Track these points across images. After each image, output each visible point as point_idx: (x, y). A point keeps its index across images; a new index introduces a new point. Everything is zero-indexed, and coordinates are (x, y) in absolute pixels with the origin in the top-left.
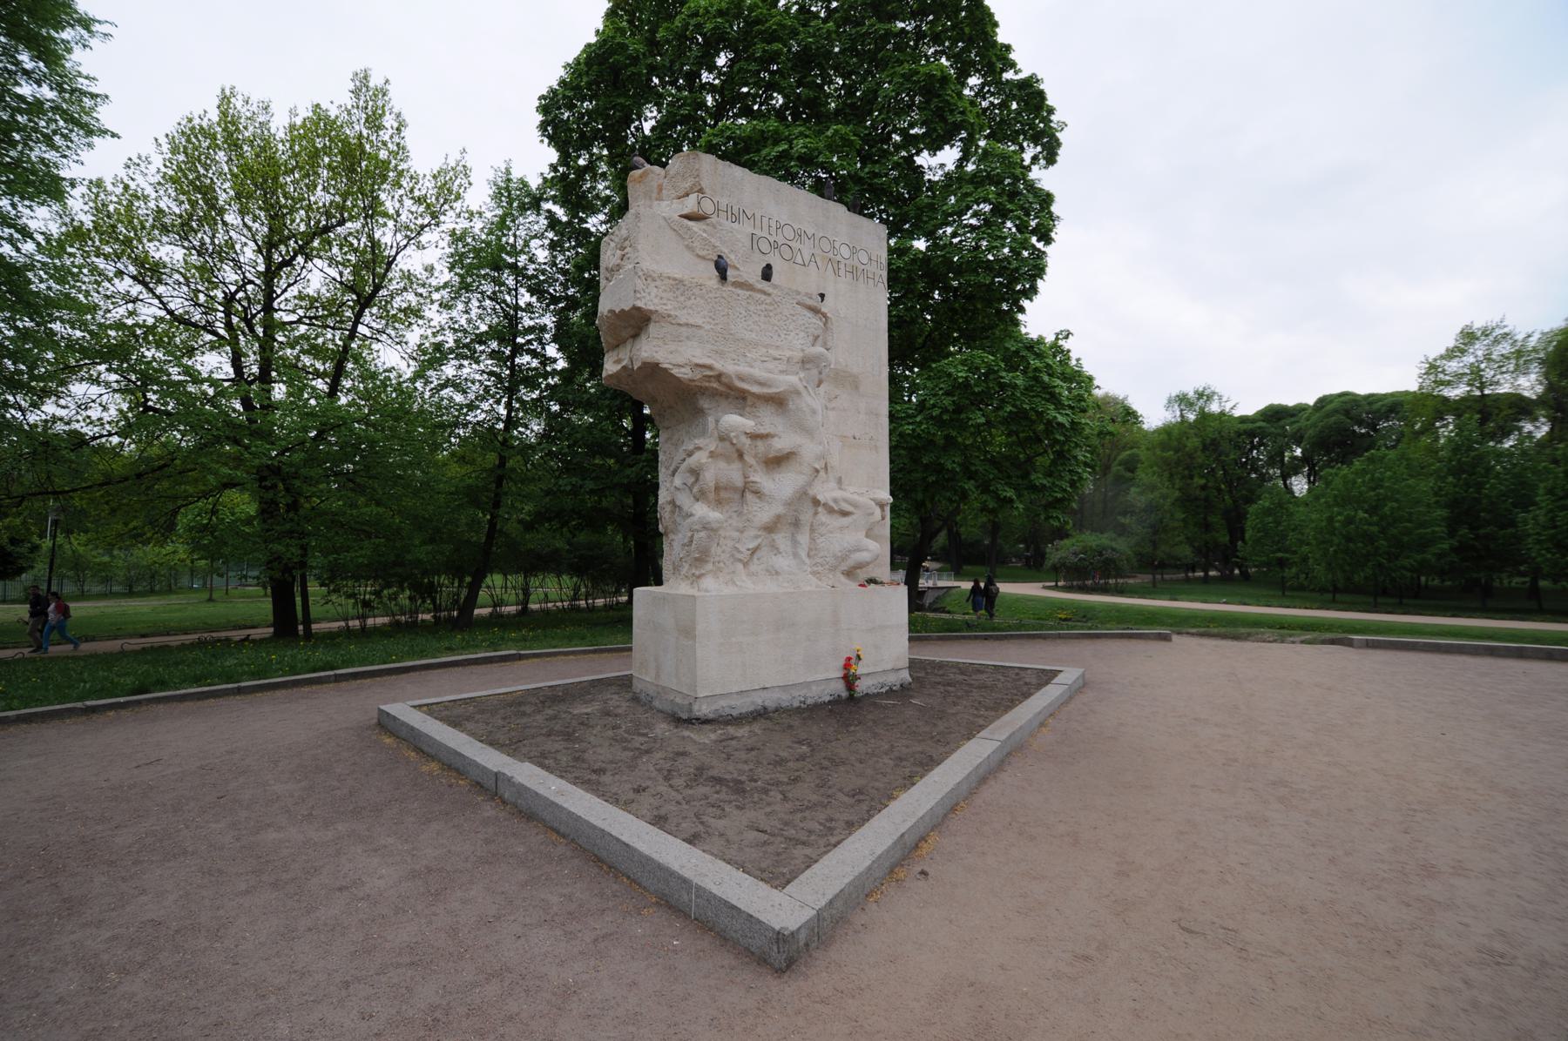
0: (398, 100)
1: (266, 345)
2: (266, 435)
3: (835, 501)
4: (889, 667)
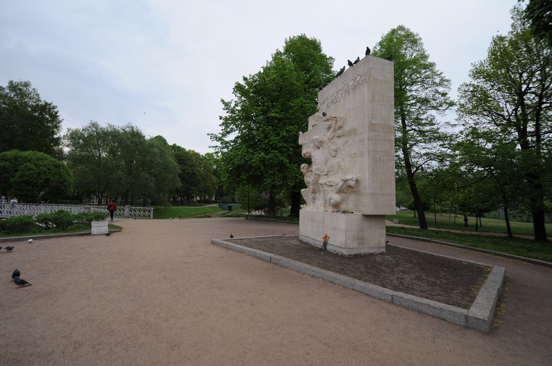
3: (329, 182)
4: (338, 245)
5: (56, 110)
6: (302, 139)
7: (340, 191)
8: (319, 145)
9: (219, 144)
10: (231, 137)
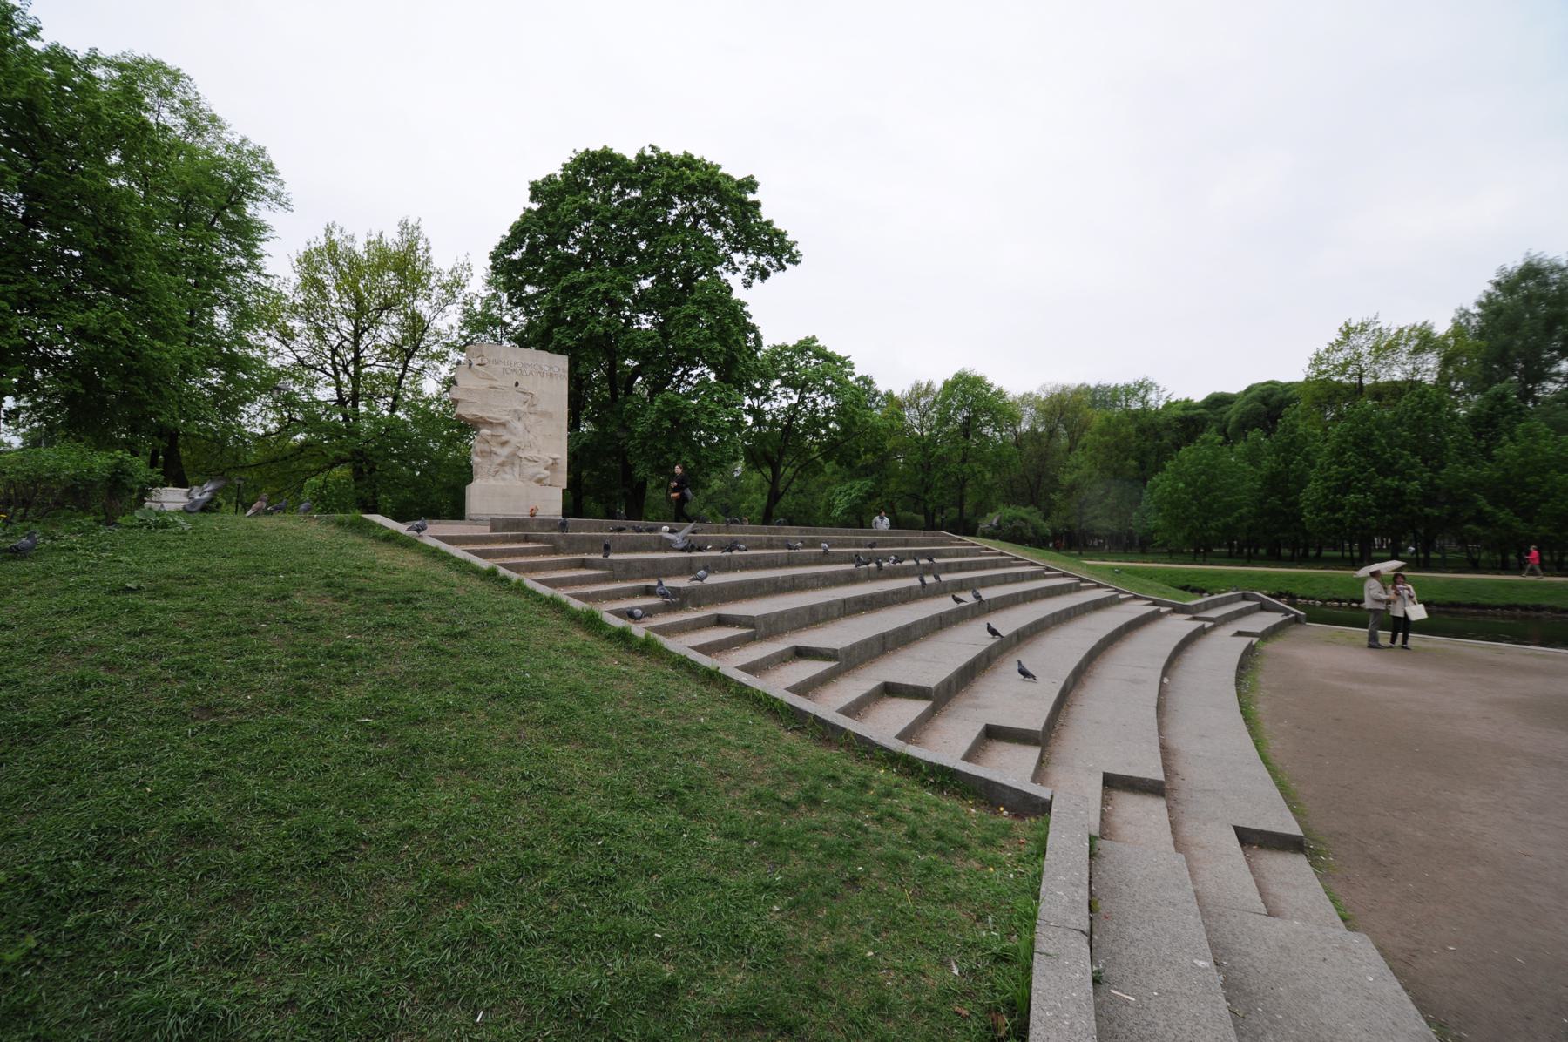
0: (426, 231)
1: (355, 380)
2: (356, 434)
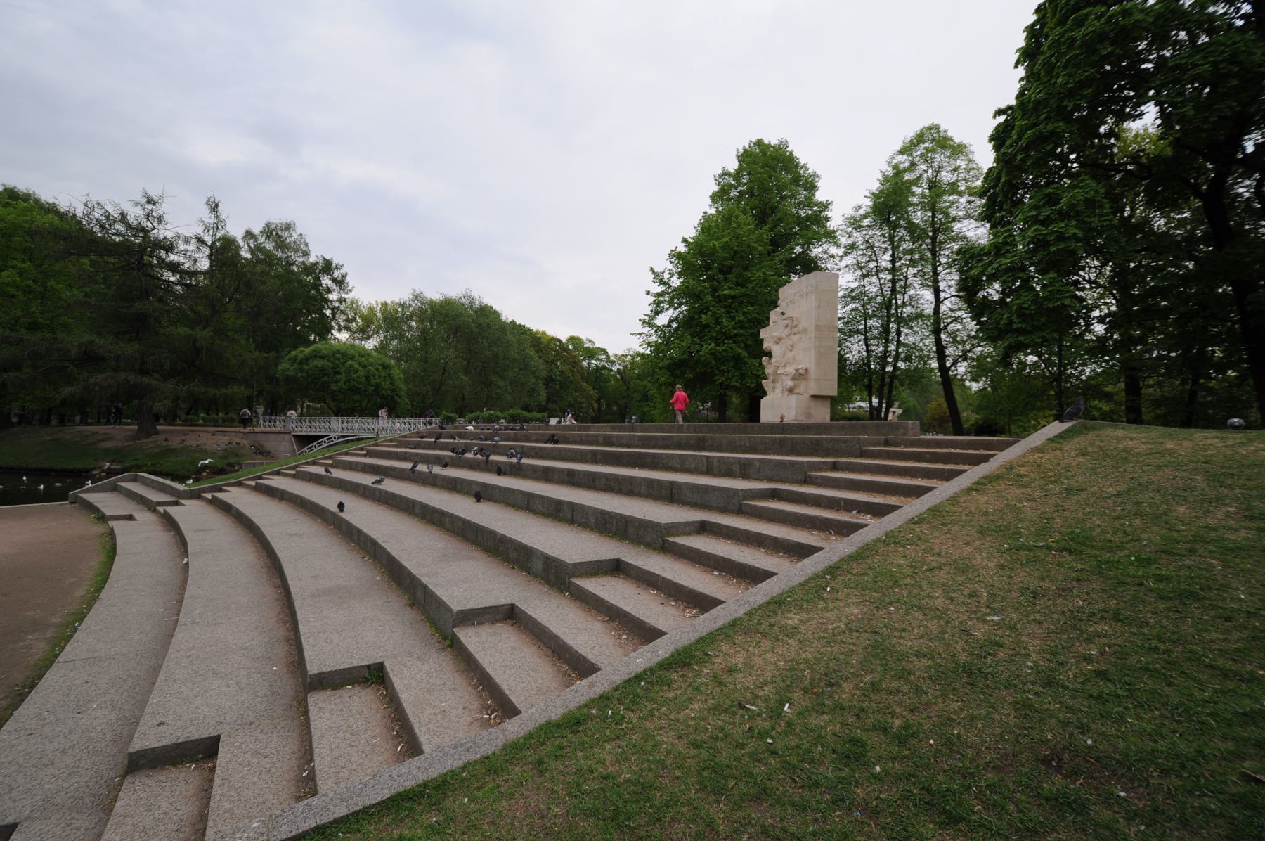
5: (343, 271)
6: (763, 333)
7: (793, 379)
8: (778, 341)
9: (646, 330)
10: (662, 320)
